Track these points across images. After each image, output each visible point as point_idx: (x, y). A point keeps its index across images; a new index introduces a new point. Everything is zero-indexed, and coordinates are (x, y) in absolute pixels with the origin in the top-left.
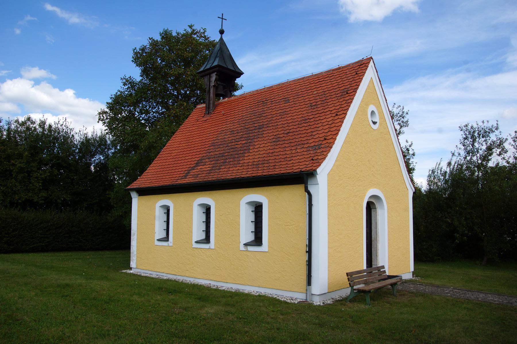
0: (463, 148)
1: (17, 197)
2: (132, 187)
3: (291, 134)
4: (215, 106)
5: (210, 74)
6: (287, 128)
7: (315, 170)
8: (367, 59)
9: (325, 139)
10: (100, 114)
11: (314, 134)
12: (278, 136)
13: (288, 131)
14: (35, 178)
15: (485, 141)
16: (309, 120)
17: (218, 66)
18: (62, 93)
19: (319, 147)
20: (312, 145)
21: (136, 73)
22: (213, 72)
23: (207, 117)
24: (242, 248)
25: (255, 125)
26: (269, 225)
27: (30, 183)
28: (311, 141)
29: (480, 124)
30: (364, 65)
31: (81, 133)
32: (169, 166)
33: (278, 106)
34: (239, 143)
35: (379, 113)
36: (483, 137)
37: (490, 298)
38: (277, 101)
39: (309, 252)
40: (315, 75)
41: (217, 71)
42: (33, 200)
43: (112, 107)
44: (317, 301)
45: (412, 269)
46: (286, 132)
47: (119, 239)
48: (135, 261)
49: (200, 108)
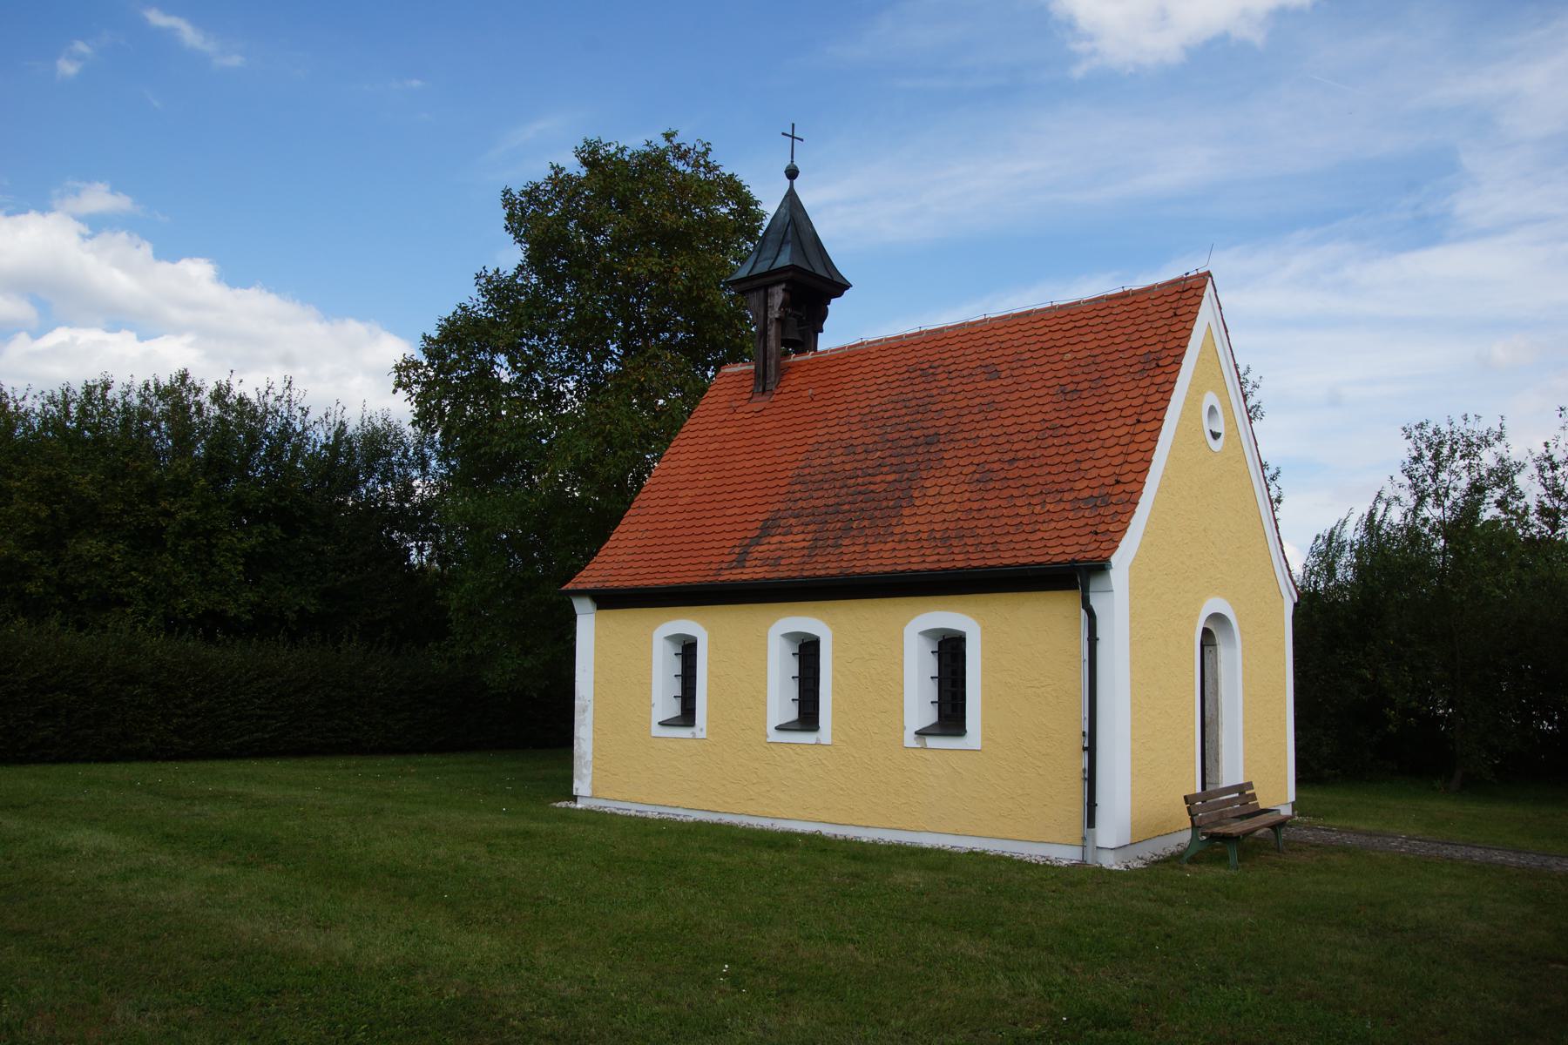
0: (1407, 482)
1: (182, 604)
2: (580, 587)
3: (1021, 464)
4: (783, 371)
5: (766, 287)
6: (1007, 446)
7: (1107, 560)
8: (1198, 276)
9: (1118, 482)
10: (398, 368)
11: (1084, 466)
12: (987, 467)
13: (1012, 455)
14: (226, 550)
15: (1470, 466)
16: (1063, 431)
17: (792, 268)
18: (165, 267)
19: (1105, 500)
20: (1086, 494)
21: (509, 257)
22: (778, 283)
23: (760, 403)
24: (910, 740)
25: (915, 434)
26: (984, 686)
27: (213, 563)
28: (1079, 485)
29: (1459, 423)
30: (1192, 292)
31: (331, 419)
32: (679, 532)
33: (971, 387)
34: (878, 479)
35: (1224, 408)
36: (1462, 457)
37: (1498, 857)
38: (965, 373)
39: (1091, 750)
40: (1061, 307)
41: (787, 282)
42: (224, 611)
43: (435, 350)
44: (1110, 862)
45: (1292, 797)
46: (1006, 457)
47: (540, 721)
48: (589, 780)
49: (733, 374)
